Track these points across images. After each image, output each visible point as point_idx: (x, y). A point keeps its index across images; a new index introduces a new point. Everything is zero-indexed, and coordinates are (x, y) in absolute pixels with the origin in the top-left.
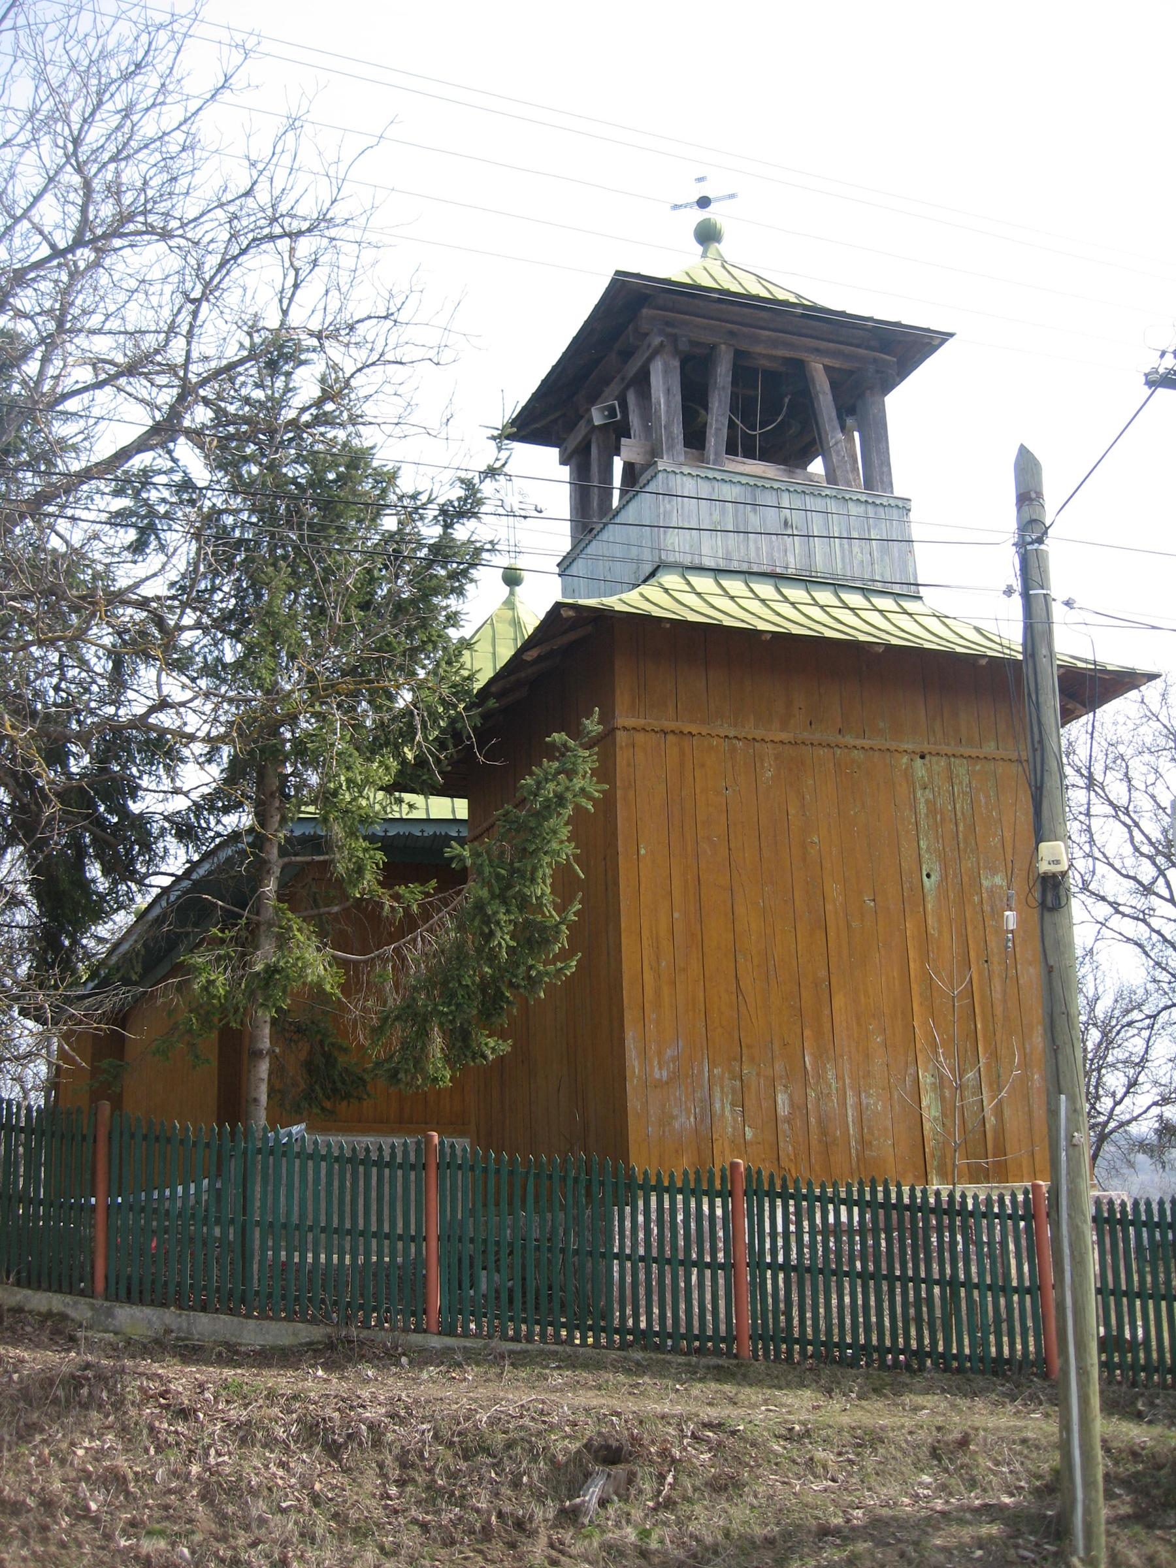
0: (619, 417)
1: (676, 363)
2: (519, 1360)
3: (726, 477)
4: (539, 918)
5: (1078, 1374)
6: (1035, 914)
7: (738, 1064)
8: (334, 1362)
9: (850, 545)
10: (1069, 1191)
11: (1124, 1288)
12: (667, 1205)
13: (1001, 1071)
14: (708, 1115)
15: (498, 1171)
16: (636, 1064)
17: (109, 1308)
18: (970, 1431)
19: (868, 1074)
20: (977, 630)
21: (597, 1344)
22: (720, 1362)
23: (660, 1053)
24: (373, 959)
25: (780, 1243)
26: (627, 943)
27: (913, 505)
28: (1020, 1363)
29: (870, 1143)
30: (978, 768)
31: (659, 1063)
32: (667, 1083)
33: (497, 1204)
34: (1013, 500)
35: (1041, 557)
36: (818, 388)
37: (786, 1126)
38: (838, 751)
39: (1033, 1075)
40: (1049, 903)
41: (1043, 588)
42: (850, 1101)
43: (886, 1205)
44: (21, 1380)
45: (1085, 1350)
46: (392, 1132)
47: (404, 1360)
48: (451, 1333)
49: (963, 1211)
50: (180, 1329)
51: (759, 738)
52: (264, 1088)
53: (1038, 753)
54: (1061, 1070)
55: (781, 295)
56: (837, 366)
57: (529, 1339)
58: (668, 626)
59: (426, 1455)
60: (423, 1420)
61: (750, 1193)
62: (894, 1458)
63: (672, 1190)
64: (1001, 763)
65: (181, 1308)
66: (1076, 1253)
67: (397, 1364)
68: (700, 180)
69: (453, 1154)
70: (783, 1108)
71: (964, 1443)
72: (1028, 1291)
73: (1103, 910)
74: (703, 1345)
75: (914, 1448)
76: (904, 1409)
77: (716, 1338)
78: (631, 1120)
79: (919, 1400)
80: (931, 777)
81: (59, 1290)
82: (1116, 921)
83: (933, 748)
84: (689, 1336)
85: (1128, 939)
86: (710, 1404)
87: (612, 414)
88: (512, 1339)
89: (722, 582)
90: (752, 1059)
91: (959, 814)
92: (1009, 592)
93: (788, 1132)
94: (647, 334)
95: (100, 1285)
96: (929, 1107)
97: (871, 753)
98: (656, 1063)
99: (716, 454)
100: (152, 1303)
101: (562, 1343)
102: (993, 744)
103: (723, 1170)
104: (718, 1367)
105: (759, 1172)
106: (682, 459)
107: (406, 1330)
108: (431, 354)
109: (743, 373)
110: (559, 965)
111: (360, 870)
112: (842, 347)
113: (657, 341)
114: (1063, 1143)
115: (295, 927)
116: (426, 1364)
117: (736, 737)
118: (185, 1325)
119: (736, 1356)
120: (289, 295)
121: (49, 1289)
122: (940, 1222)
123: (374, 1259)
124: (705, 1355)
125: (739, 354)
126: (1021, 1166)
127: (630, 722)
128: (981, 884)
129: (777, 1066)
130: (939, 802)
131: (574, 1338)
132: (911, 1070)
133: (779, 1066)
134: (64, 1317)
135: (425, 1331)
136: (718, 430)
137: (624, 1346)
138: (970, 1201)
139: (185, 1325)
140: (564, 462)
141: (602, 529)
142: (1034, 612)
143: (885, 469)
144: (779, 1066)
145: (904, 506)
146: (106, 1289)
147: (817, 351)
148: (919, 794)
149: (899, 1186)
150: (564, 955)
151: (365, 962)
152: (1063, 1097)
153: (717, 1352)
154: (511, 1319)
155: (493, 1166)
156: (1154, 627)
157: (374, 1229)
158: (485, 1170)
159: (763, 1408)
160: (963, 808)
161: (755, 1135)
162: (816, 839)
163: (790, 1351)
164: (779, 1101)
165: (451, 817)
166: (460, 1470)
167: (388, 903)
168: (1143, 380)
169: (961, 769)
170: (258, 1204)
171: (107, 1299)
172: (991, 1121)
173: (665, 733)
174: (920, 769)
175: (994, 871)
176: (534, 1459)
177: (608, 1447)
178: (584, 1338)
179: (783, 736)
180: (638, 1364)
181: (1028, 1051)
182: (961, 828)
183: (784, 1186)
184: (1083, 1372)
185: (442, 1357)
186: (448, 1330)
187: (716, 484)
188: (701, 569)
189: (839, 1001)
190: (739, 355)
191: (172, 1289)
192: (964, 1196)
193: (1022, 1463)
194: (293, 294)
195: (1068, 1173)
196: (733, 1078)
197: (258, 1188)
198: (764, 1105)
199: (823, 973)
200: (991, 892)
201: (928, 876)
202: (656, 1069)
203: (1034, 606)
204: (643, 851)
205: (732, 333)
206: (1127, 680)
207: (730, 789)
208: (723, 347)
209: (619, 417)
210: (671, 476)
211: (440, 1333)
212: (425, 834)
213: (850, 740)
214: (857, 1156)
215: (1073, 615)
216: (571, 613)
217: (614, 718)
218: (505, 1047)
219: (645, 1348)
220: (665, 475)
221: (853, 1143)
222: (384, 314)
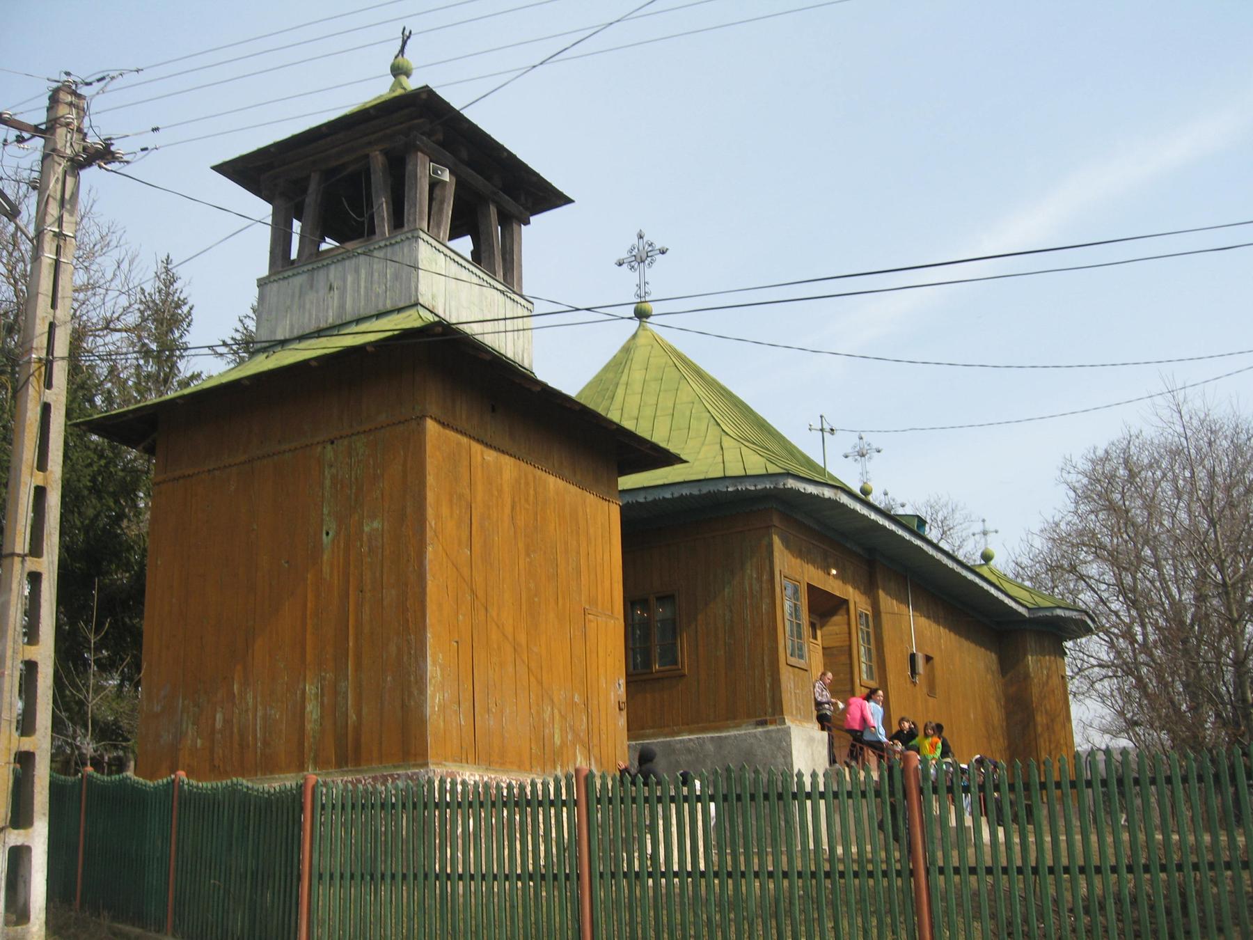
33: (200, 799)
39: (387, 677)
42: (259, 714)
96: (312, 712)
140: (527, 223)
147: (370, 144)
162: (255, 527)
165: (744, 474)
174: (329, 452)
201: (327, 534)
212: (648, 500)
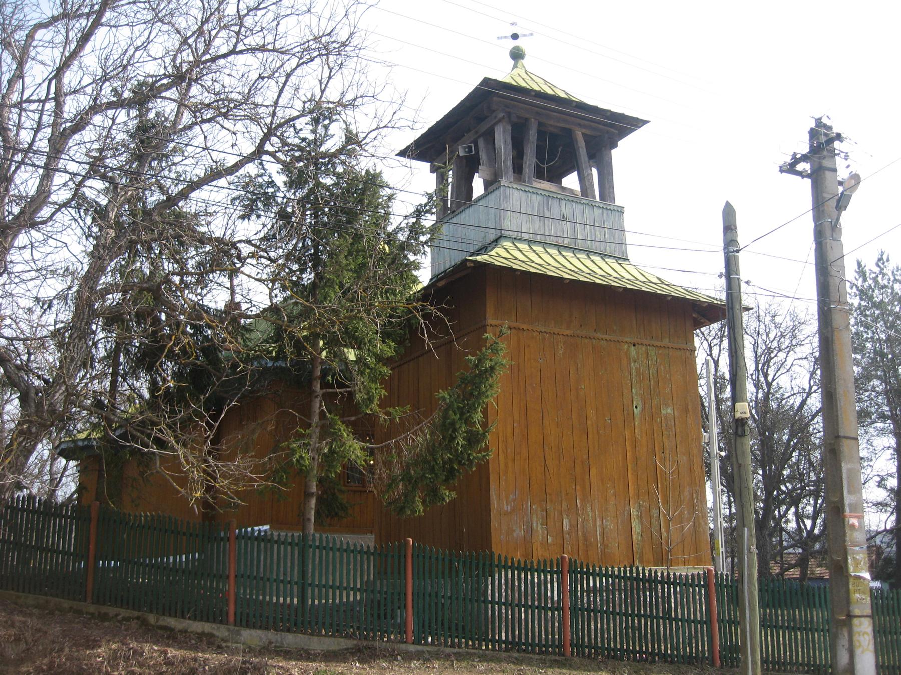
0: (473, 153)
2: (459, 657)
3: (534, 191)
4: (474, 429)
5: (753, 665)
8: (363, 659)
9: (595, 230)
11: (497, 600)
12: (509, 576)
14: (530, 531)
15: (444, 560)
17: (238, 631)
19: (607, 509)
20: (658, 278)
21: (493, 649)
23: (507, 497)
24: (382, 447)
27: (626, 210)
28: (689, 657)
32: (510, 513)
34: (722, 230)
35: (736, 259)
40: (740, 433)
42: (598, 524)
43: (637, 579)
44: (210, 670)
47: (399, 658)
48: (419, 644)
49: (655, 581)
50: (277, 642)
51: (556, 333)
52: (313, 513)
57: (459, 647)
61: (571, 572)
63: (532, 571)
65: (275, 630)
67: (397, 660)
68: (513, 24)
69: (327, 542)
70: (566, 528)
72: (705, 623)
74: (547, 650)
80: (638, 356)
81: (208, 621)
83: (639, 341)
87: (470, 151)
88: (451, 647)
89: (533, 247)
90: (551, 501)
91: (651, 376)
92: (720, 276)
94: (494, 111)
95: (232, 619)
99: (529, 178)
100: (260, 628)
101: (476, 649)
102: (667, 340)
103: (557, 560)
104: (555, 661)
105: (575, 561)
106: (512, 180)
108: (410, 124)
109: (541, 134)
110: (484, 454)
111: (370, 400)
113: (501, 115)
114: (746, 551)
115: (342, 429)
116: (412, 660)
118: (279, 640)
120: (325, 83)
121: (201, 620)
122: (650, 586)
123: (331, 601)
125: (540, 125)
129: (563, 506)
130: (642, 369)
131: (482, 646)
132: (627, 508)
133: (564, 505)
134: (211, 636)
136: (530, 165)
138: (659, 575)
139: (279, 640)
143: (611, 191)
144: (564, 505)
145: (620, 211)
146: (235, 621)
148: (632, 365)
151: (377, 448)
153: (554, 653)
154: (450, 636)
155: (441, 557)
156: (787, 297)
157: (331, 584)
158: (437, 559)
162: (583, 387)
164: (564, 523)
167: (383, 417)
168: (779, 169)
169: (652, 352)
170: (310, 575)
171: (235, 626)
174: (633, 351)
175: (667, 406)
178: (487, 646)
179: (568, 332)
180: (516, 659)
182: (652, 383)
183: (512, 563)
184: (754, 663)
185: (418, 656)
186: (417, 642)
187: (529, 194)
188: (521, 240)
189: (593, 472)
191: (271, 621)
192: (656, 572)
194: (328, 83)
195: (748, 566)
197: (310, 567)
198: (557, 525)
200: (666, 417)
201: (636, 408)
203: (733, 284)
205: (538, 114)
208: (533, 120)
209: (473, 153)
210: (507, 189)
211: (413, 644)
216: (472, 265)
217: (485, 319)
218: (454, 495)
219: (518, 651)
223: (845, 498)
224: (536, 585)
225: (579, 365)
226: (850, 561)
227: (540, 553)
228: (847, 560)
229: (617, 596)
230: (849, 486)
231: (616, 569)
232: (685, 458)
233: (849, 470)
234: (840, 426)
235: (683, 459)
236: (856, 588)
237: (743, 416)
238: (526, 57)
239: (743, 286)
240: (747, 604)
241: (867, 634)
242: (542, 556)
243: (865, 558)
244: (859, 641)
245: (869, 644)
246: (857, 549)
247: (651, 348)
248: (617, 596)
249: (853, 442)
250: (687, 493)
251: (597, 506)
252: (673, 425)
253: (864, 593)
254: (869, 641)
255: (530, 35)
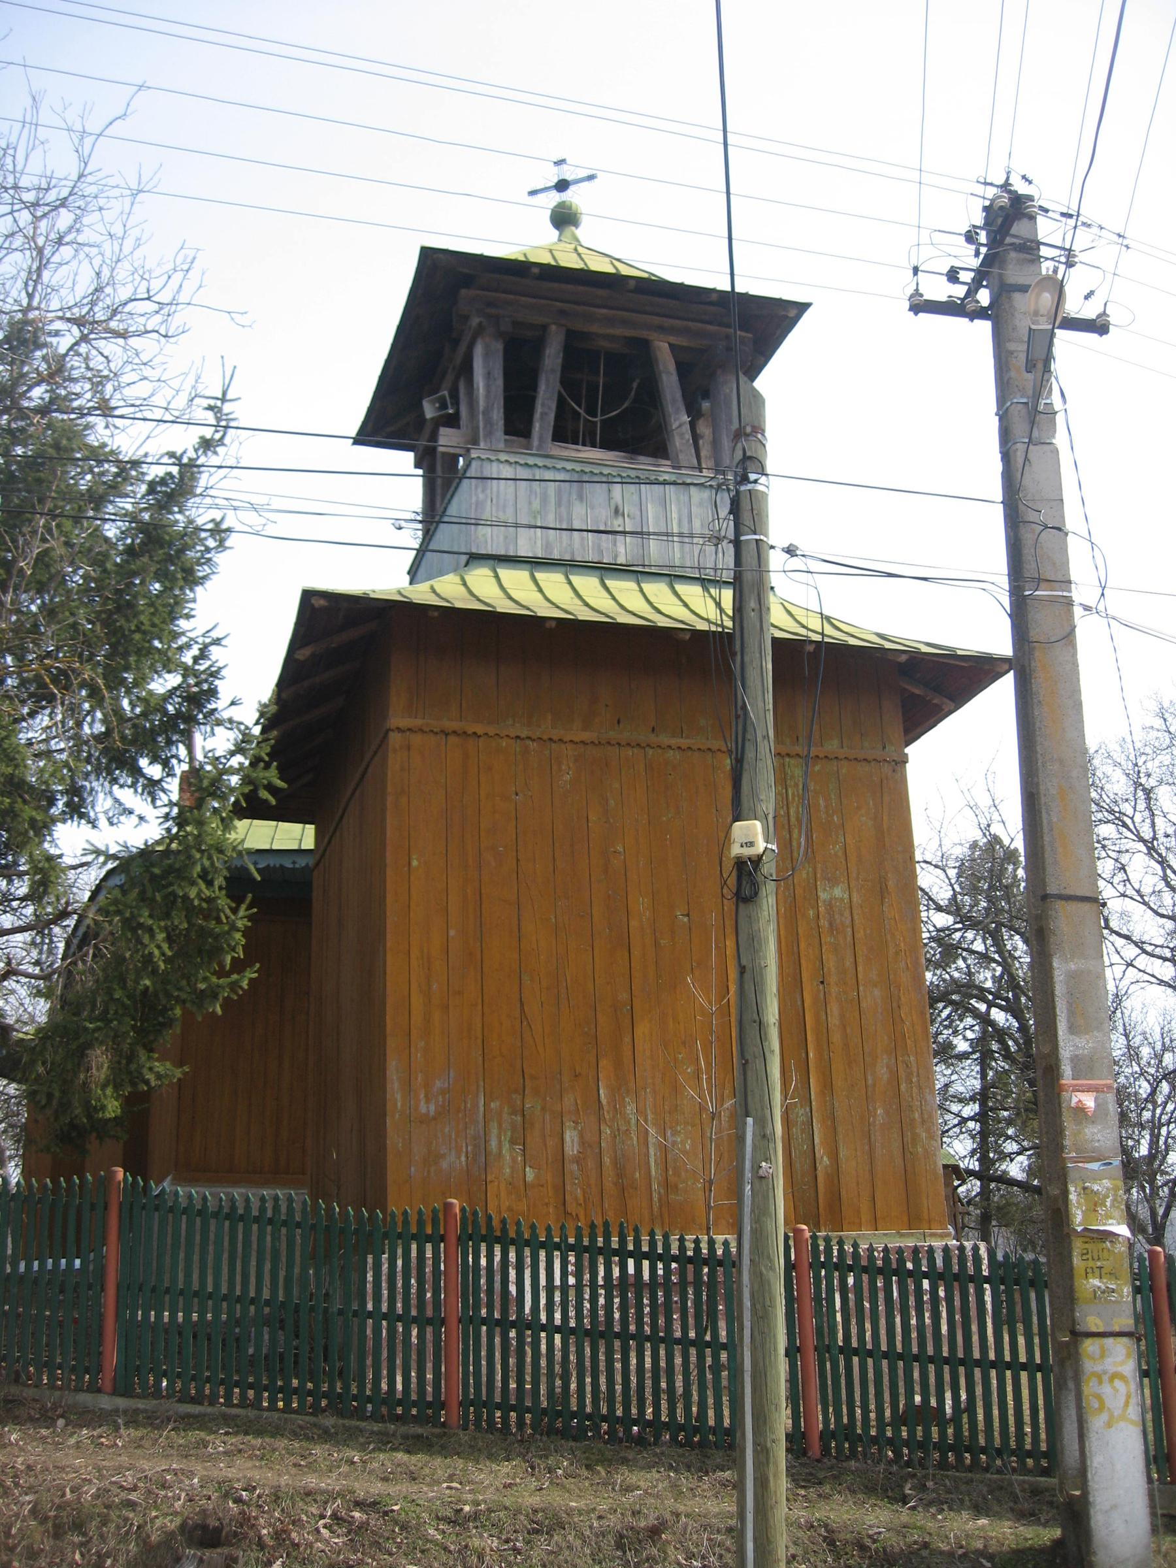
1: (499, 346)
3: (549, 462)
6: (729, 905)
7: (520, 1097)
10: (754, 1232)
13: (836, 1105)
14: (482, 1158)
16: (399, 1097)
18: (668, 1516)
21: (287, 1409)
22: (420, 1430)
25: (557, 1298)
26: (392, 963)
29: (676, 1186)
30: (817, 768)
31: (426, 1096)
32: (434, 1119)
36: (661, 368)
37: (575, 1167)
38: (650, 752)
39: (875, 1109)
41: (755, 533)
45: (765, 1422)
46: (265, 1184)
51: (555, 738)
53: (741, 721)
54: (749, 1089)
55: (625, 271)
56: (685, 344)
57: (256, 1405)
58: (436, 614)
59: (14, 1531)
60: (30, 1490)
62: (570, 1548)
64: (845, 763)
66: (758, 1306)
68: (560, 163)
70: (572, 1145)
71: (654, 1532)
73: (1131, 951)
75: (597, 1536)
76: (613, 1489)
77: (421, 1402)
78: (390, 1157)
79: (633, 1478)
82: (1143, 961)
84: (421, 1402)
85: (1162, 981)
86: (385, 1479)
91: (793, 819)
93: (577, 1173)
97: (690, 753)
98: (422, 1096)
99: (541, 439)
102: (836, 742)
103: (434, 1211)
104: (419, 1437)
106: (501, 446)
107: (78, 1390)
112: (690, 324)
113: (475, 321)
114: (748, 1175)
117: (529, 738)
119: (444, 1425)
124: (404, 1424)
126: (859, 1212)
127: (404, 723)
128: (817, 897)
135: (99, 1391)
136: (543, 414)
137: (317, 1410)
141: (436, 528)
142: (744, 560)
147: (661, 329)
149: (652, 1234)
150: (239, 966)
152: (750, 1120)
159: (445, 1485)
160: (797, 812)
161: (537, 1177)
162: (620, 848)
163: (506, 1419)
166: (42, 1550)
172: (824, 1161)
173: (447, 735)
175: (833, 881)
176: (124, 1539)
177: (204, 1527)
178: (273, 1401)
179: (586, 736)
180: (326, 1431)
181: (870, 1082)
189: (642, 1029)
190: (573, 339)
193: (721, 1556)
195: (752, 1211)
196: (514, 1113)
199: (624, 996)
200: (830, 905)
202: (422, 1103)
203: (744, 553)
204: (415, 863)
205: (562, 312)
206: (987, 667)
207: (521, 795)
208: (553, 327)
212: (297, 866)
213: (665, 739)
214: (660, 1200)
215: (795, 563)
216: (323, 602)
219: (341, 1414)
220: (479, 463)
221: (655, 1186)
222: (146, 296)
223: (1061, 1044)
224: (483, 1273)
225: (612, 802)
226: (1073, 1197)
227: (506, 1204)
228: (1065, 1193)
229: (691, 1296)
230: (1072, 1013)
231: (645, 1238)
232: (877, 992)
233: (1073, 976)
234: (1050, 870)
235: (873, 997)
236: (1091, 1263)
237: (747, 852)
238: (585, 221)
239: (776, 560)
240: (747, 1303)
241: (1122, 1377)
242: (510, 1209)
243: (1116, 1189)
244: (1099, 1397)
245: (1127, 1404)
246: (1095, 1166)
247: (793, 761)
248: (691, 1296)
249: (1086, 907)
250: (882, 1072)
251: (650, 1101)
252: (848, 922)
253: (1113, 1275)
254: (1128, 1397)
255: (591, 178)
